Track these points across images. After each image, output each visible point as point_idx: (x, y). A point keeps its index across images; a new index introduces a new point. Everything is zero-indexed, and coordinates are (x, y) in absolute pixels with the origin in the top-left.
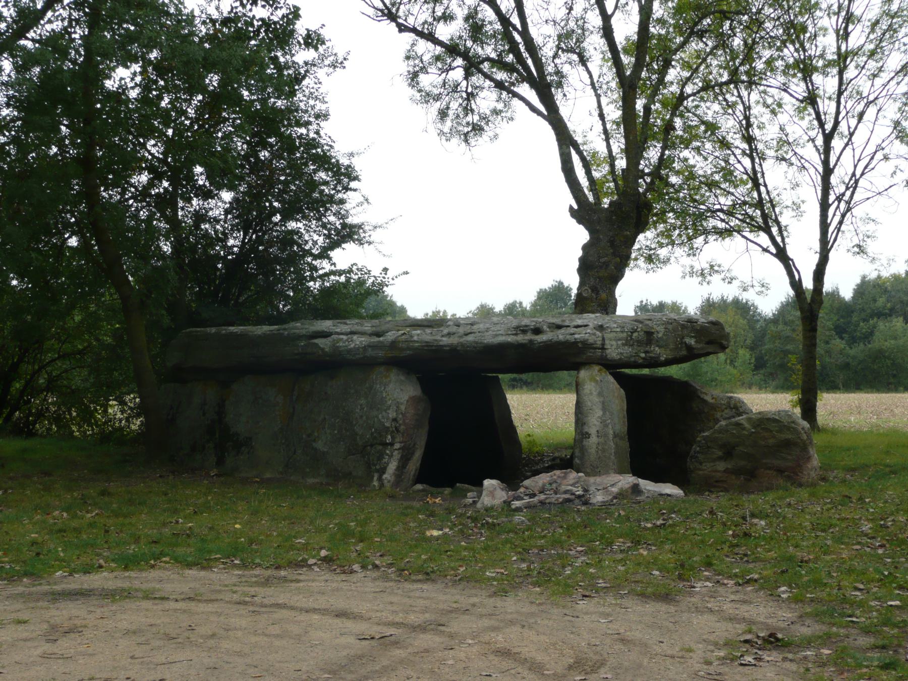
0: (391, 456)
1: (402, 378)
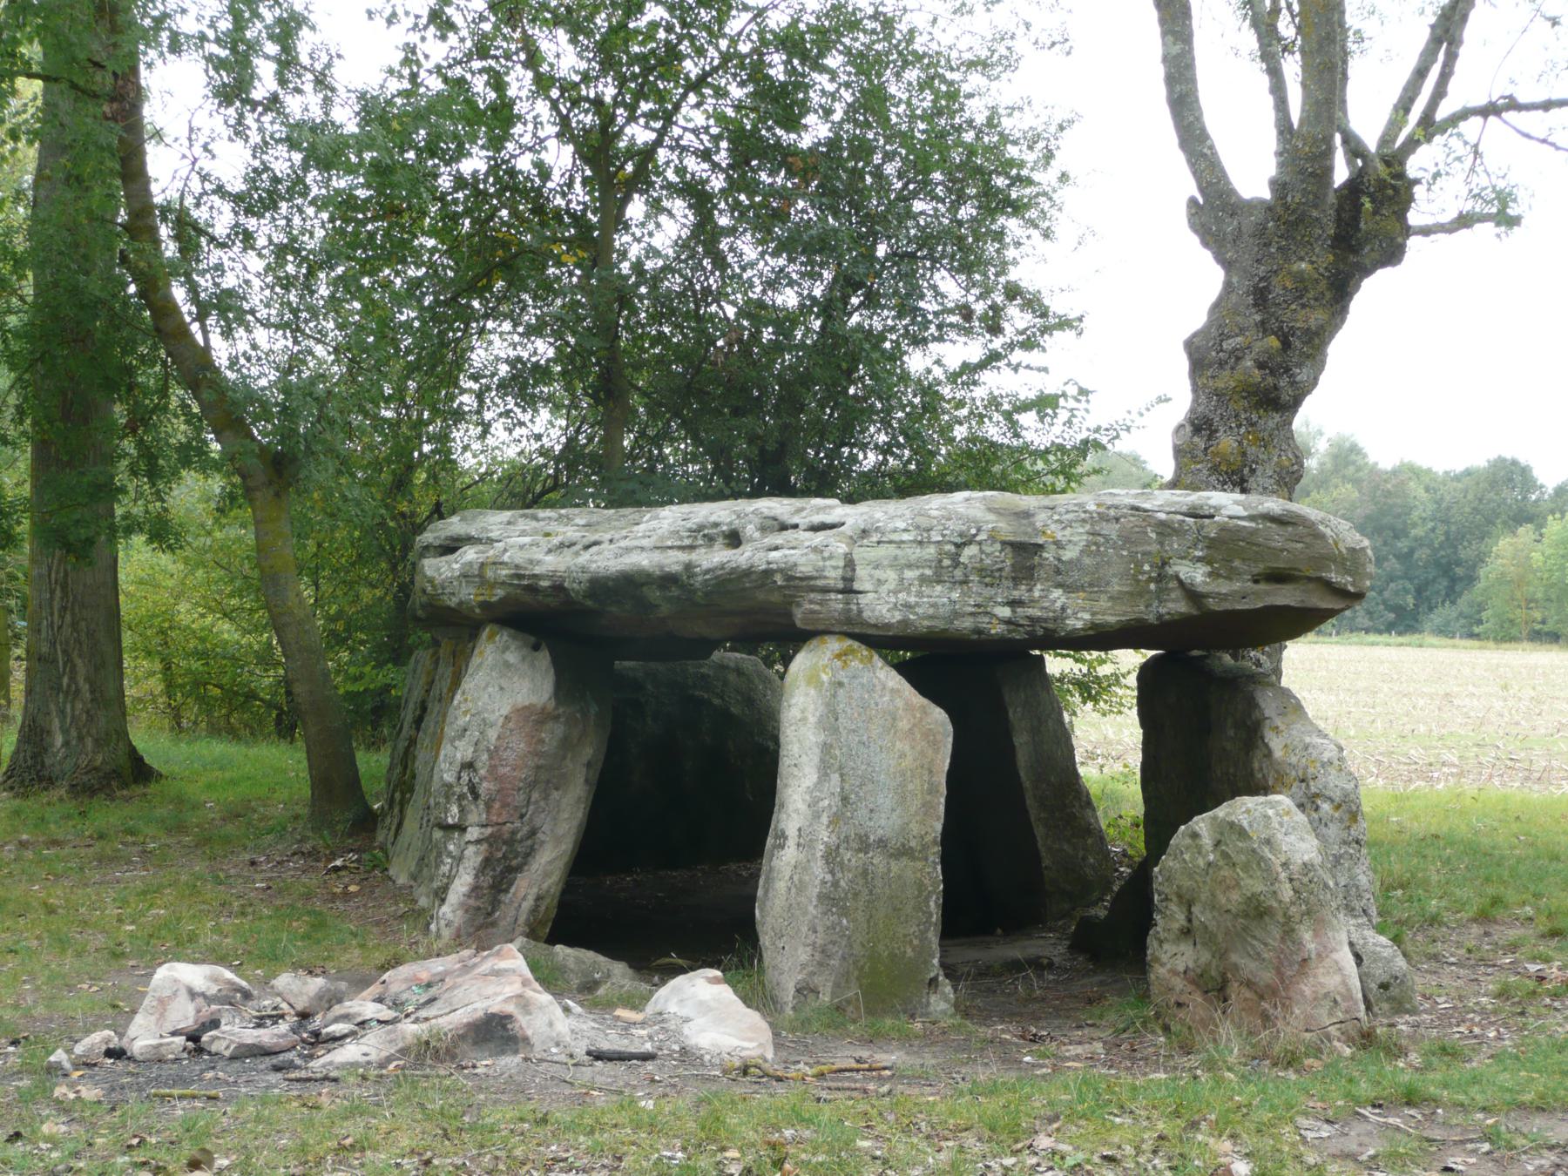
0: (459, 859)
1: (512, 657)
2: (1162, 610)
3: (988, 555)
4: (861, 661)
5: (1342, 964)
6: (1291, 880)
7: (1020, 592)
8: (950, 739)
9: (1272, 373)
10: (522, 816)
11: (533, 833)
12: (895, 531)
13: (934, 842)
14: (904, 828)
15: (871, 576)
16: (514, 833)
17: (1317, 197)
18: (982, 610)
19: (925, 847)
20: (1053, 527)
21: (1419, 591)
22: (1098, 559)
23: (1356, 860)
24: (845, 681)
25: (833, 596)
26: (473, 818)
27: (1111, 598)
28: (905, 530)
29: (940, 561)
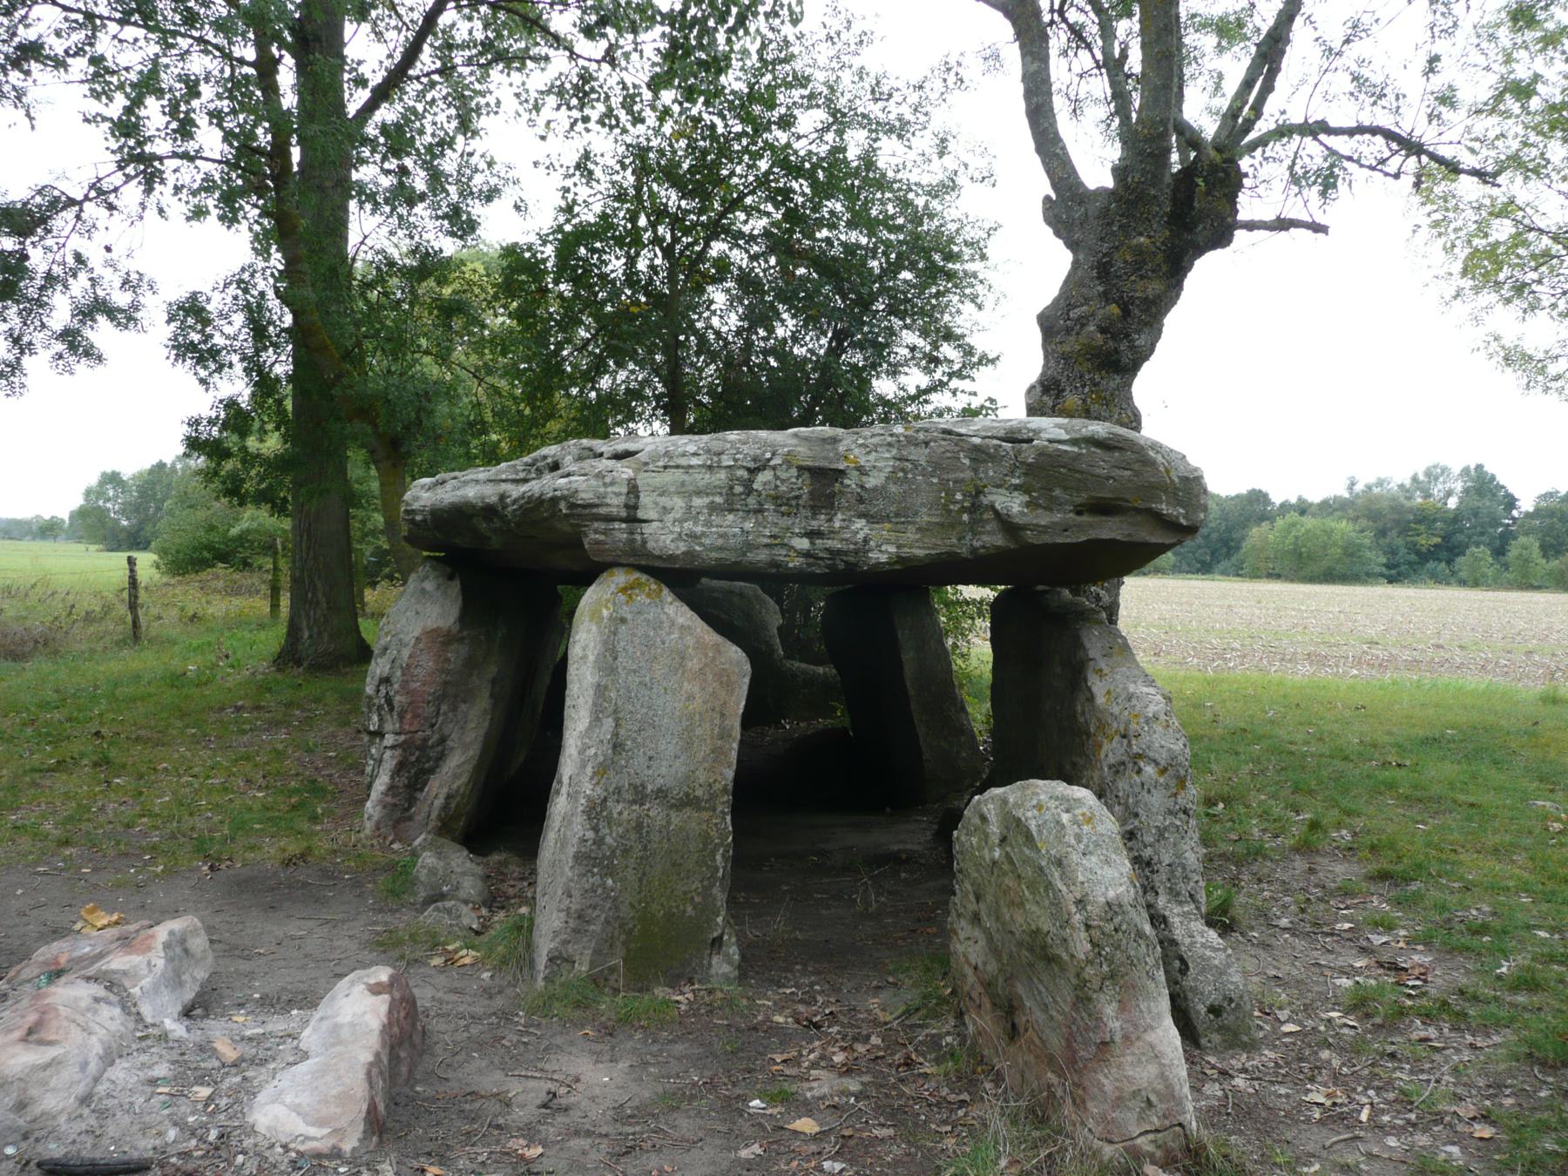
0: (380, 761)
1: (429, 586)
2: (976, 544)
3: (783, 481)
4: (649, 596)
5: (1160, 1048)
6: (1088, 927)
7: (820, 522)
8: (747, 680)
9: (1114, 337)
10: (433, 726)
11: (443, 740)
12: (684, 455)
13: (725, 790)
14: (689, 777)
15: (656, 503)
16: (425, 740)
17: (1154, 176)
18: (777, 541)
19: (713, 797)
20: (857, 451)
21: (1213, 554)
22: (906, 487)
23: (1182, 833)
24: (629, 616)
25: (616, 525)
26: (388, 727)
27: (919, 530)
28: (695, 454)
29: (731, 488)
